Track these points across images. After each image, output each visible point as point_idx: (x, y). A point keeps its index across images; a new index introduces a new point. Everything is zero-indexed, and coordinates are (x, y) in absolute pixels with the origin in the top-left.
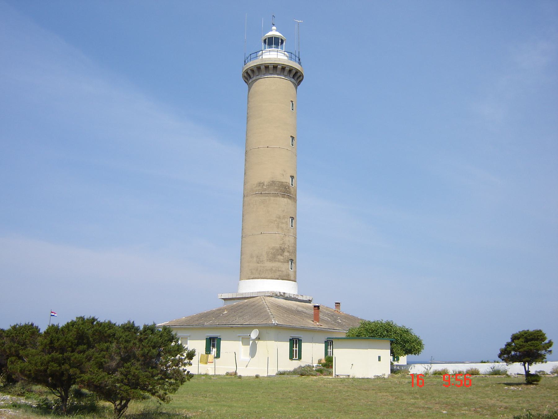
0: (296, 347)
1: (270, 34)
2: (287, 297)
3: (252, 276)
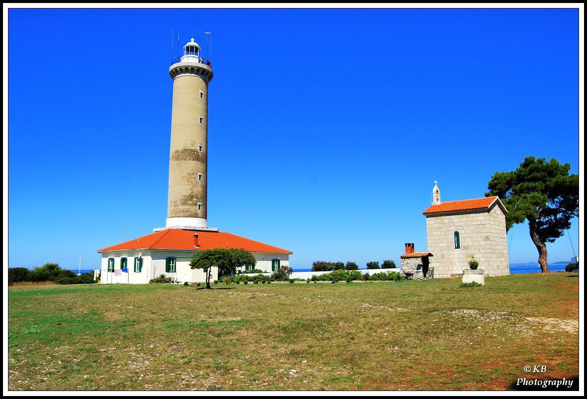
0: (173, 263)
1: (189, 44)
2: (466, 284)
3: (172, 216)
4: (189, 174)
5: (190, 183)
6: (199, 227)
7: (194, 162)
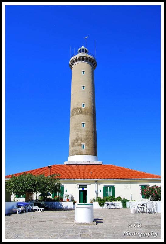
4: (76, 125)
5: (76, 131)
6: (81, 162)
7: (79, 115)
